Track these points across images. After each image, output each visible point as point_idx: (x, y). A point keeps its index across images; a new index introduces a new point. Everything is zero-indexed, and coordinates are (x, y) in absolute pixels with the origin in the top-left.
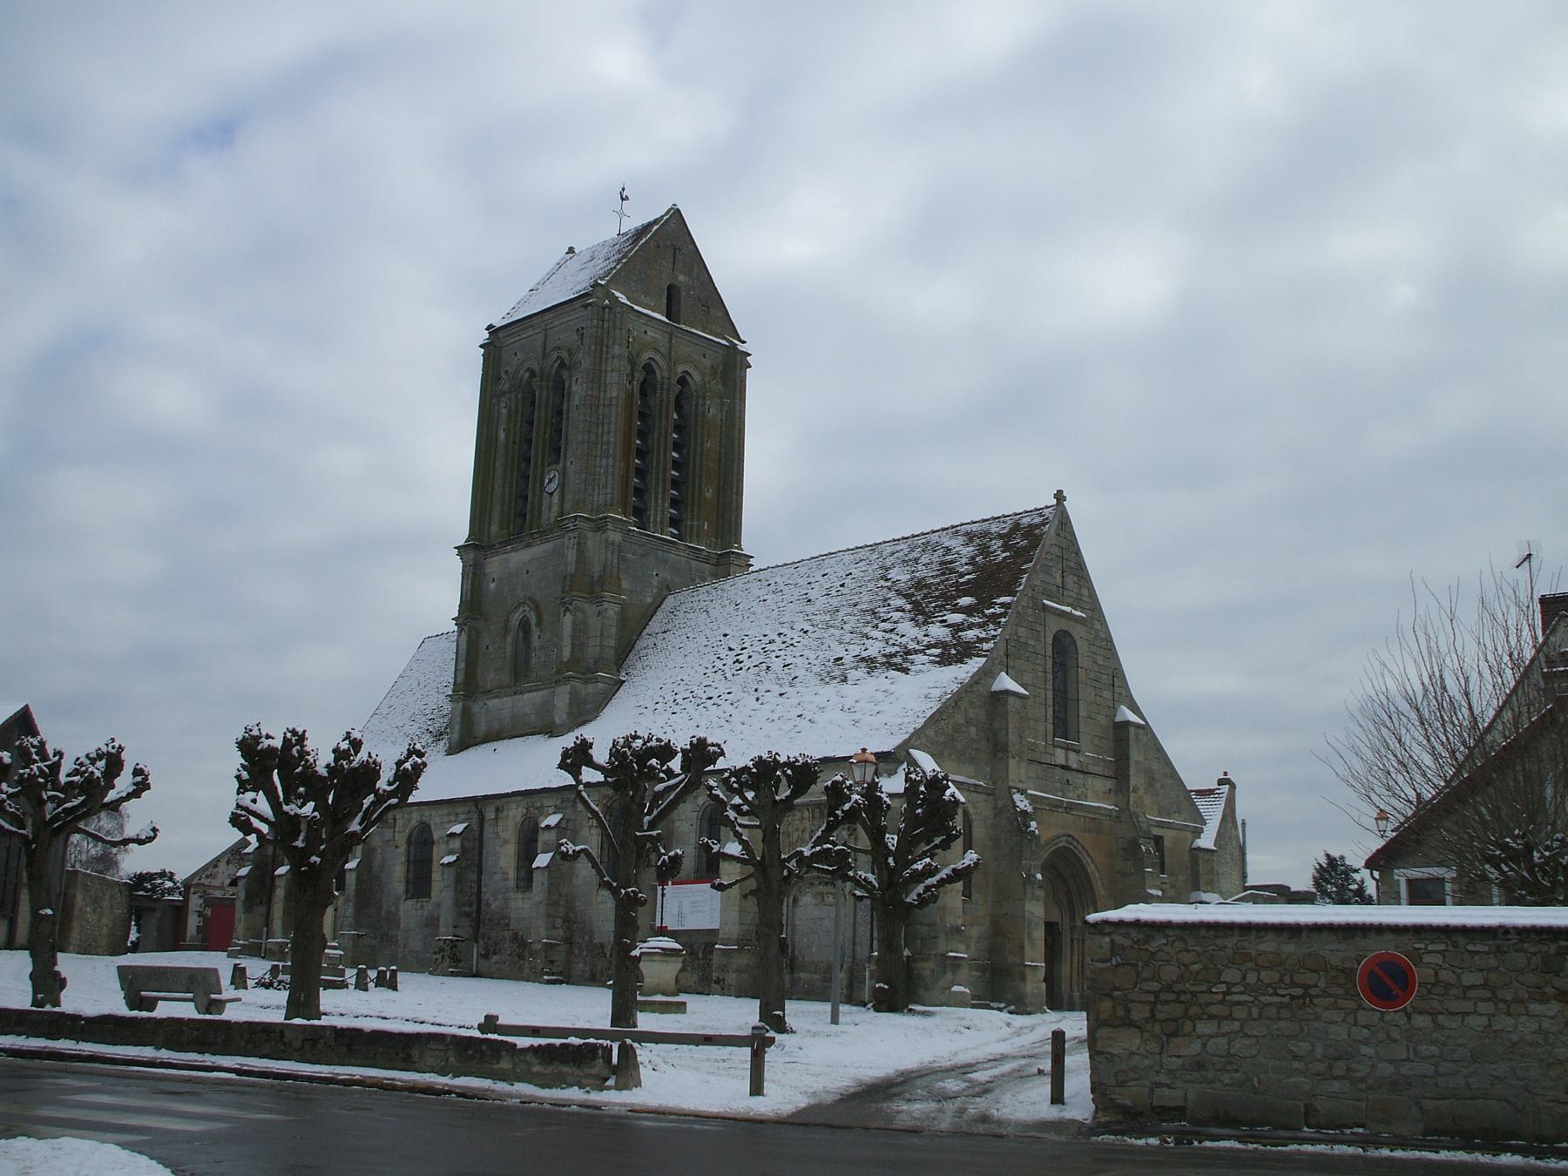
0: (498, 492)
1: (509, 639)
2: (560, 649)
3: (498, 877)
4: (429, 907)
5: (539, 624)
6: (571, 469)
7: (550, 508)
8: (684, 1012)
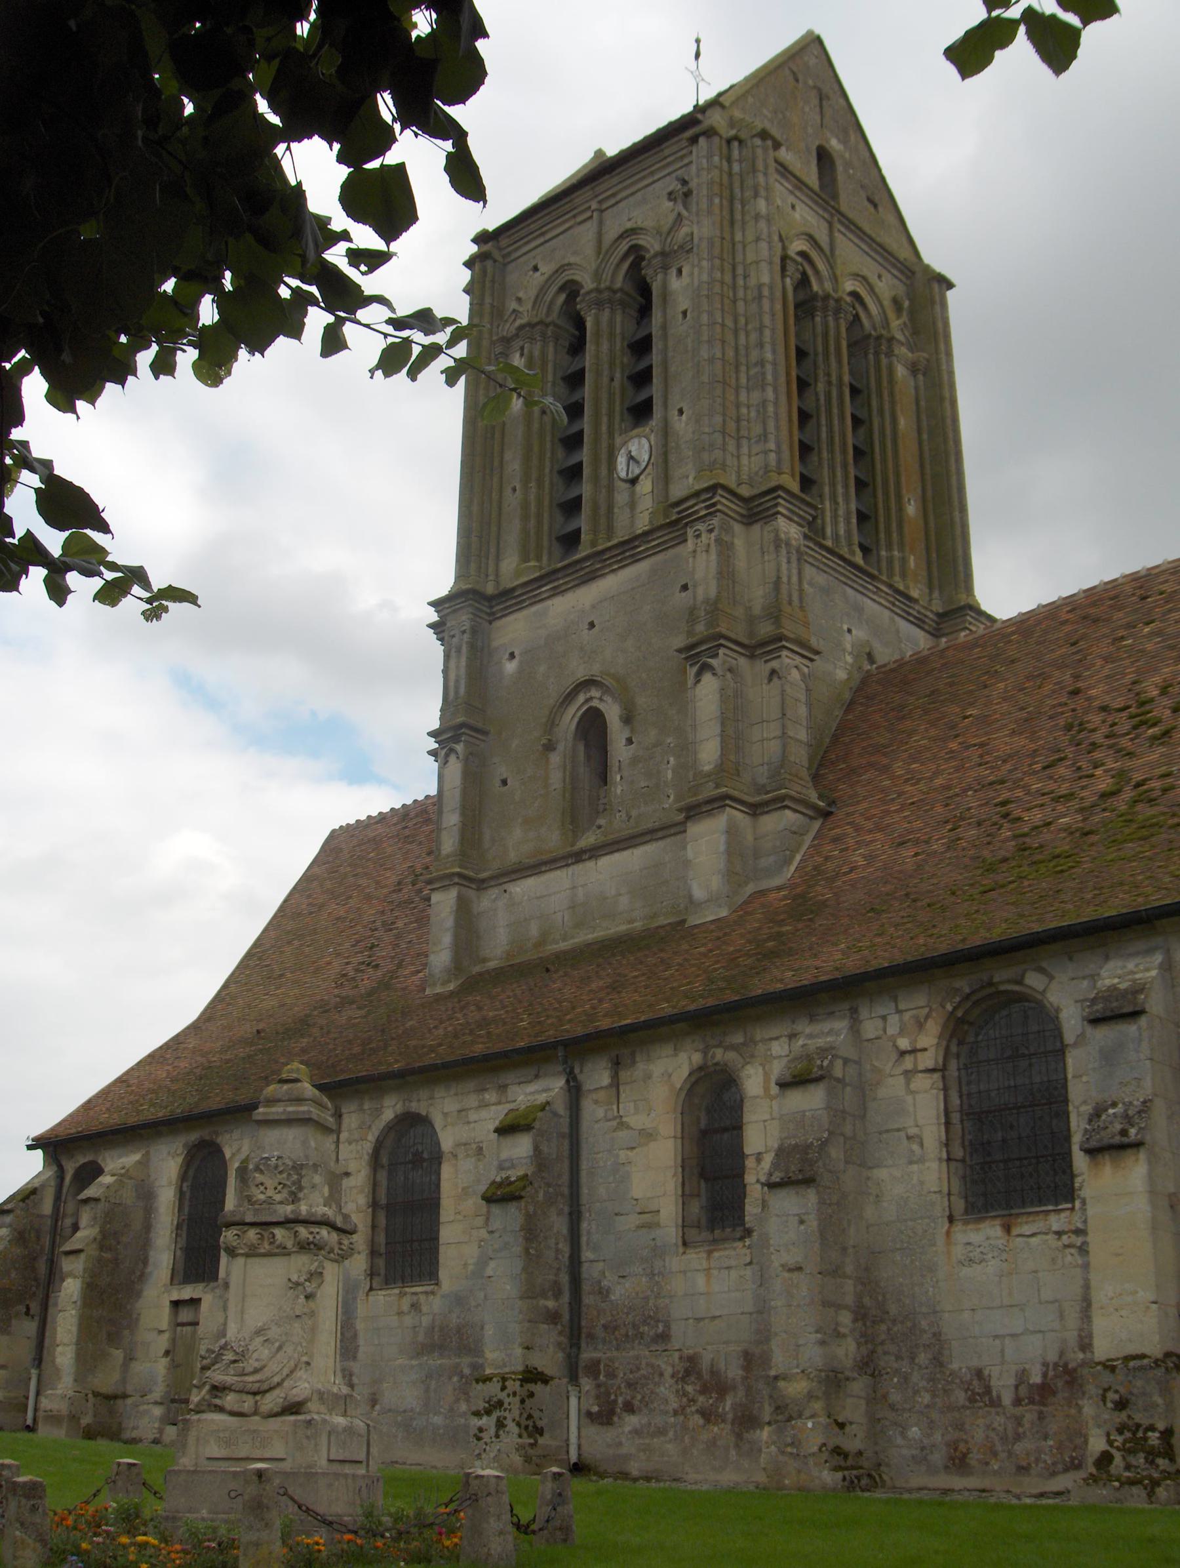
0: (512, 501)
1: (555, 759)
2: (686, 748)
3: (633, 1220)
4: (433, 1306)
5: (627, 720)
6: (681, 426)
7: (632, 505)
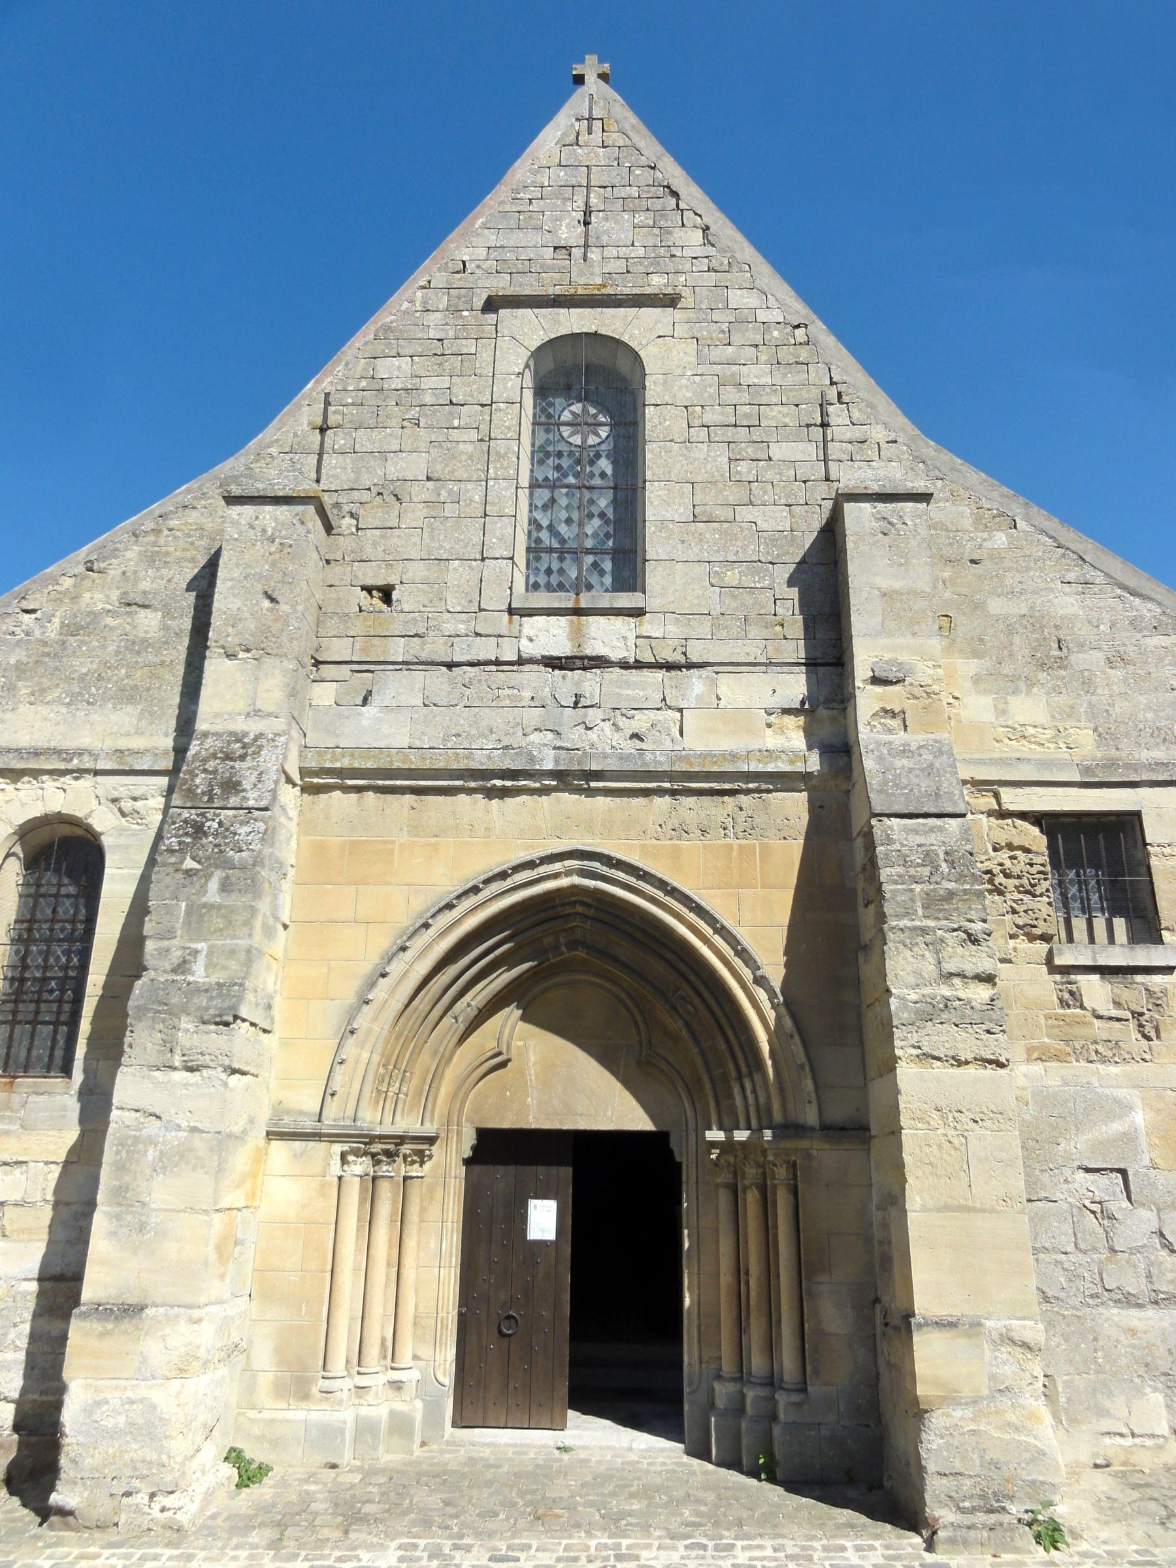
8: (484, 1135)
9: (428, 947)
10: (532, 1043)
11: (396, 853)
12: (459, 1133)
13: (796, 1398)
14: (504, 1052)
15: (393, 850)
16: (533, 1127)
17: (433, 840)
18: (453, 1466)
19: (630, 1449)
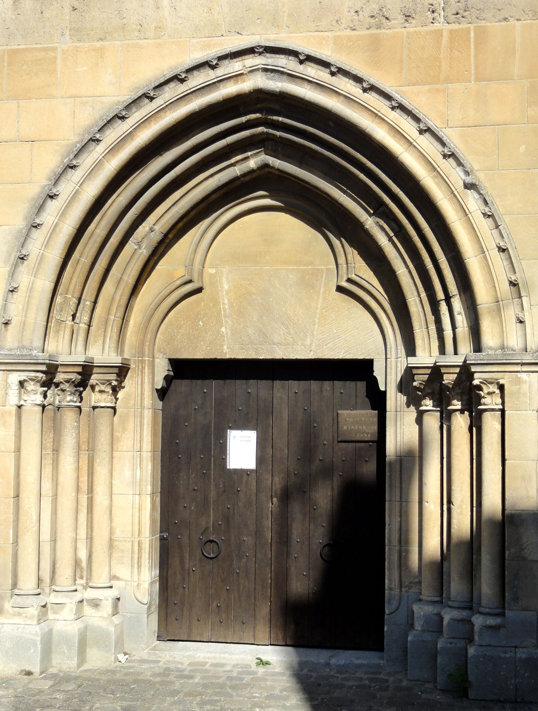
9: (98, 165)
10: (225, 270)
11: (59, 61)
12: (152, 365)
13: (492, 621)
14: (195, 279)
15: (55, 58)
16: (228, 357)
17: (98, 44)
18: (147, 675)
19: (328, 665)
